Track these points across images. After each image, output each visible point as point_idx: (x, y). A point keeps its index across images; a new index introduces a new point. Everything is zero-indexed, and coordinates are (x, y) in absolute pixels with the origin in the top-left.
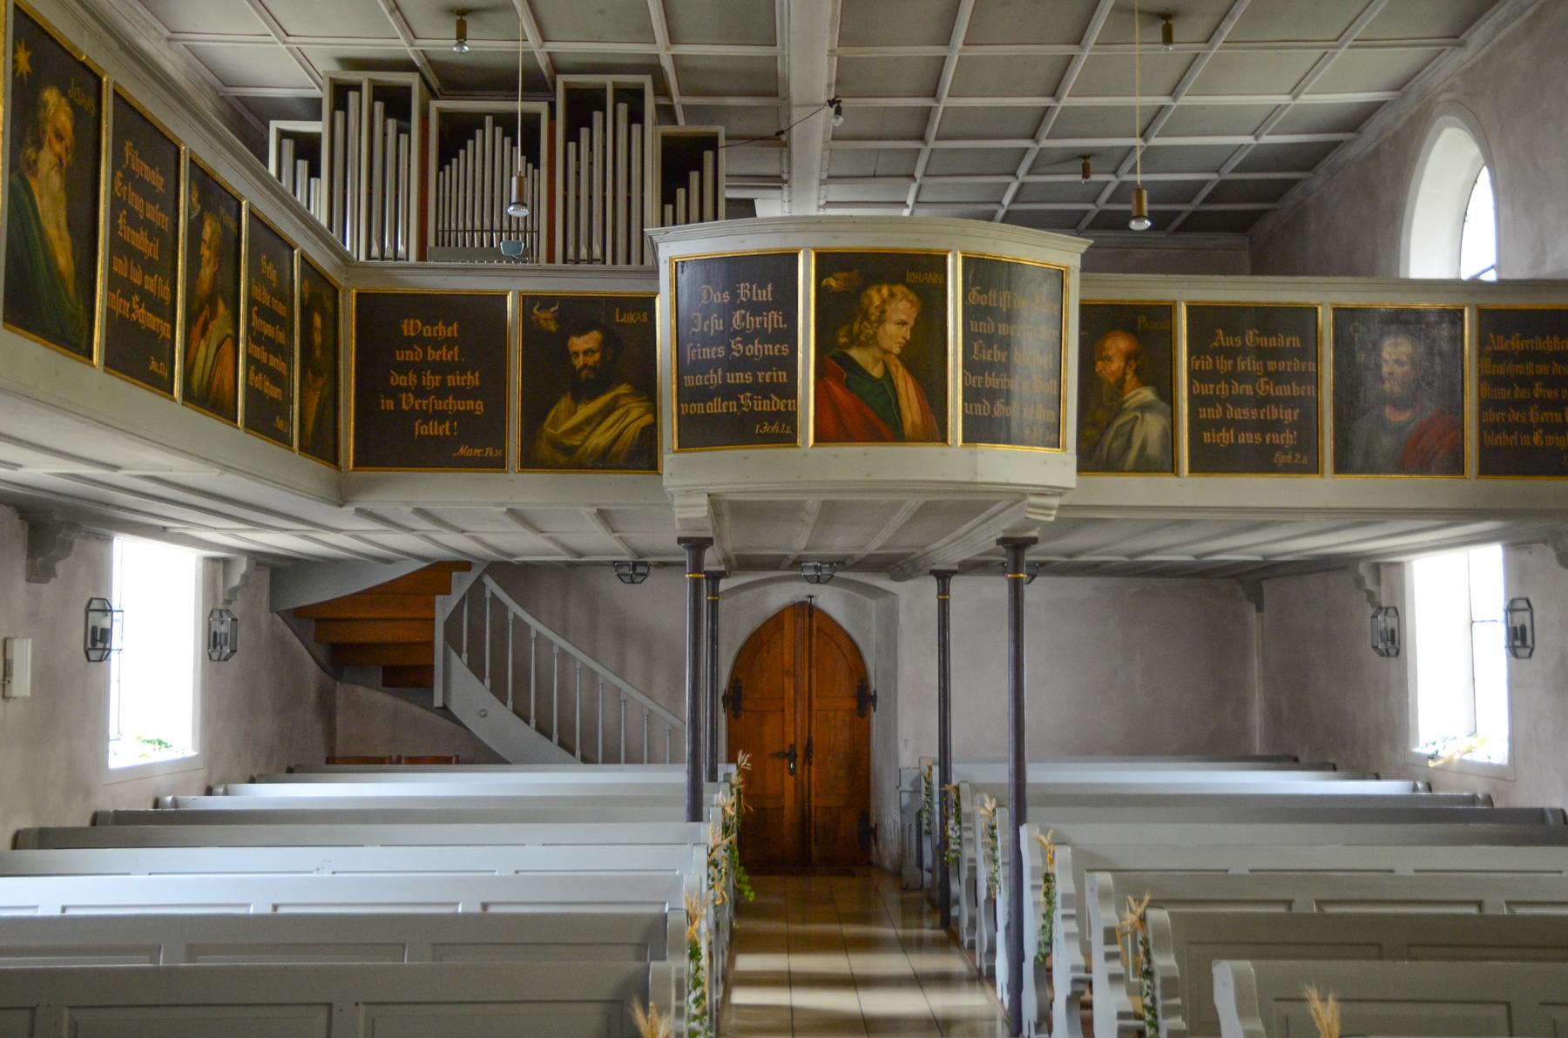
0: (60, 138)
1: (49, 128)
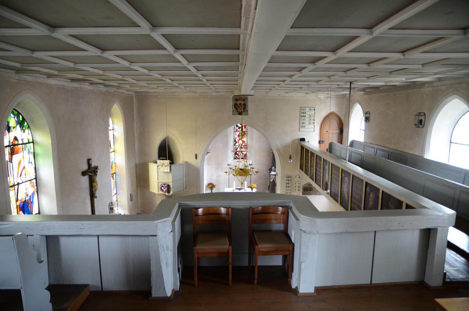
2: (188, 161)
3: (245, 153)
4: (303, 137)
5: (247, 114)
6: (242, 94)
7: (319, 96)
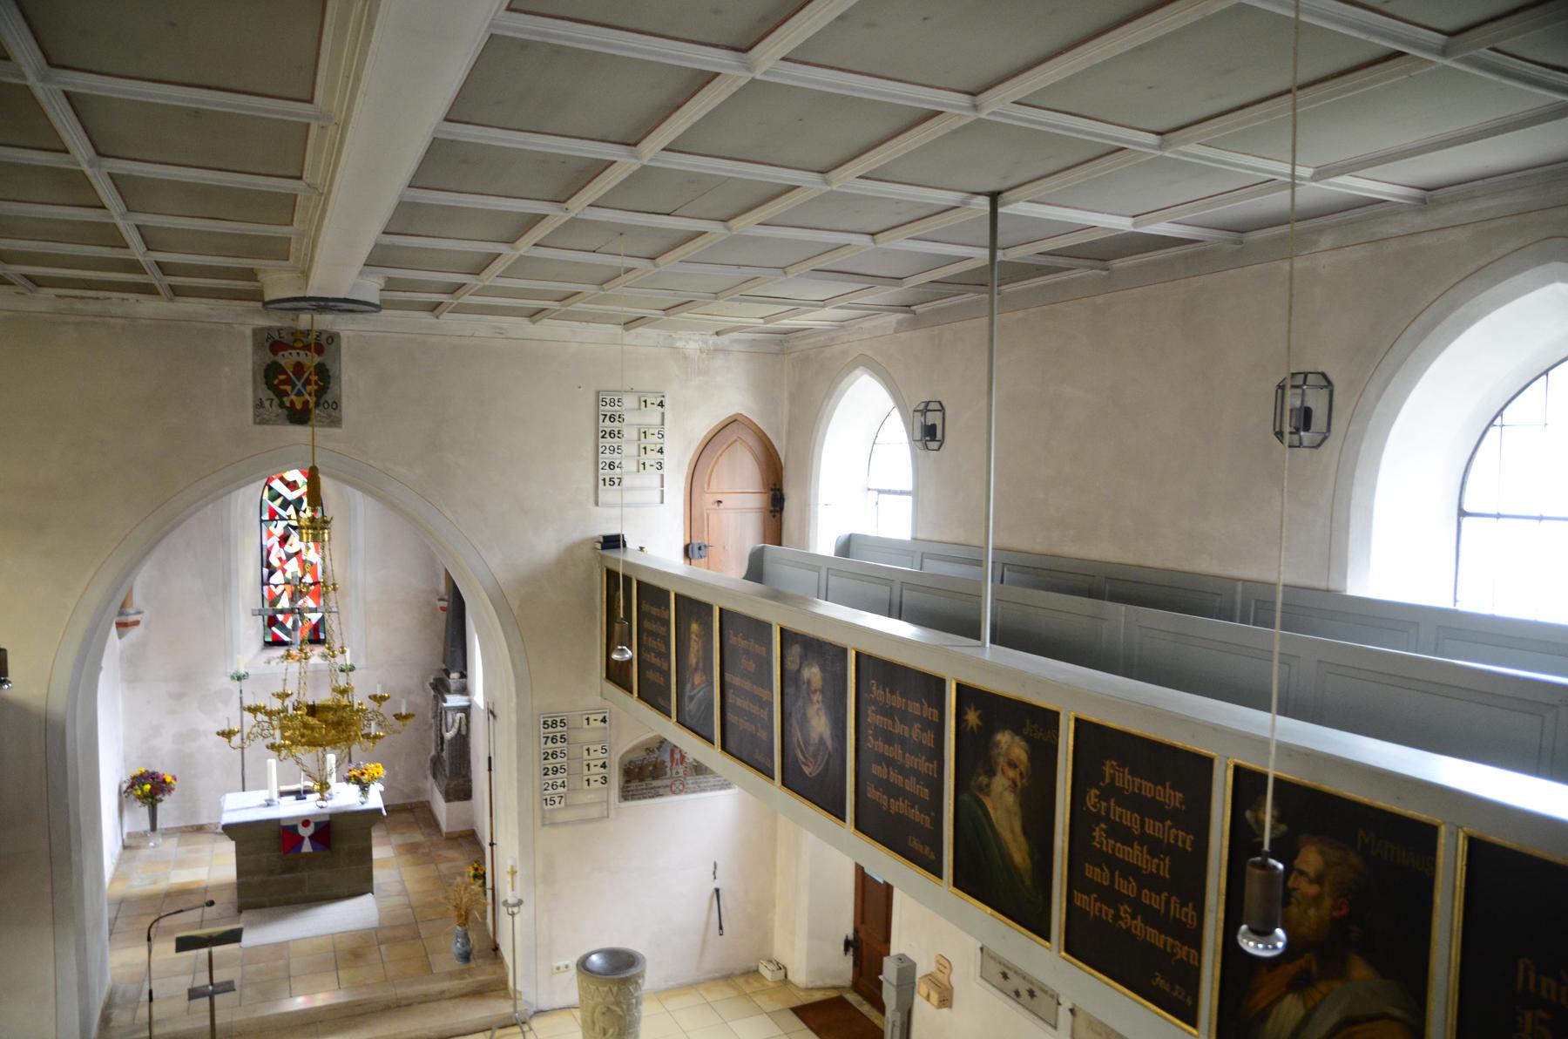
0: (1013, 765)
1: (1001, 761)
3: (314, 617)
4: (612, 530)
5: (335, 422)
6: (310, 293)
7: (679, 344)
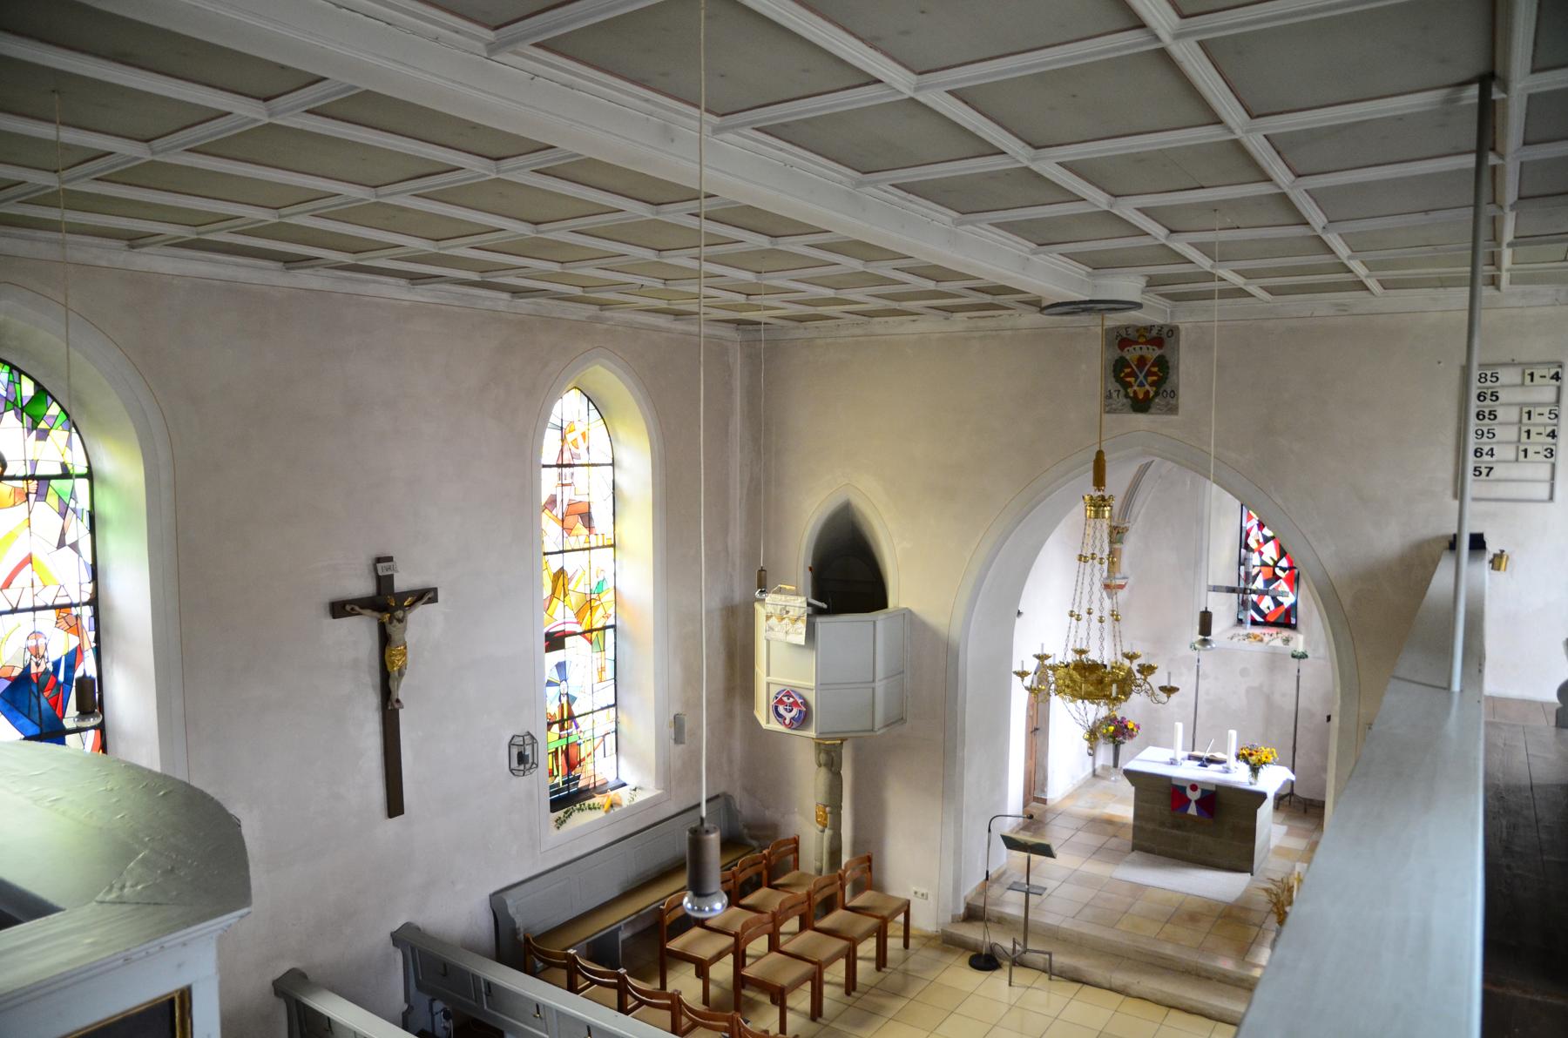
2: (915, 608)
3: (1287, 601)
5: (1173, 410)
